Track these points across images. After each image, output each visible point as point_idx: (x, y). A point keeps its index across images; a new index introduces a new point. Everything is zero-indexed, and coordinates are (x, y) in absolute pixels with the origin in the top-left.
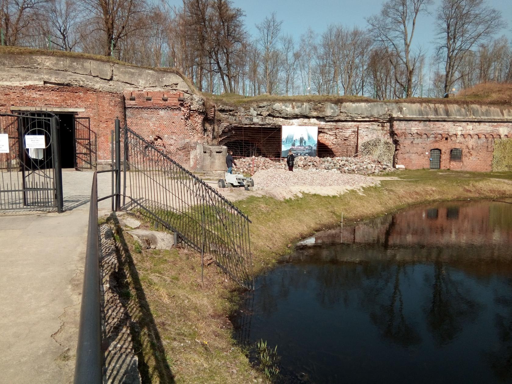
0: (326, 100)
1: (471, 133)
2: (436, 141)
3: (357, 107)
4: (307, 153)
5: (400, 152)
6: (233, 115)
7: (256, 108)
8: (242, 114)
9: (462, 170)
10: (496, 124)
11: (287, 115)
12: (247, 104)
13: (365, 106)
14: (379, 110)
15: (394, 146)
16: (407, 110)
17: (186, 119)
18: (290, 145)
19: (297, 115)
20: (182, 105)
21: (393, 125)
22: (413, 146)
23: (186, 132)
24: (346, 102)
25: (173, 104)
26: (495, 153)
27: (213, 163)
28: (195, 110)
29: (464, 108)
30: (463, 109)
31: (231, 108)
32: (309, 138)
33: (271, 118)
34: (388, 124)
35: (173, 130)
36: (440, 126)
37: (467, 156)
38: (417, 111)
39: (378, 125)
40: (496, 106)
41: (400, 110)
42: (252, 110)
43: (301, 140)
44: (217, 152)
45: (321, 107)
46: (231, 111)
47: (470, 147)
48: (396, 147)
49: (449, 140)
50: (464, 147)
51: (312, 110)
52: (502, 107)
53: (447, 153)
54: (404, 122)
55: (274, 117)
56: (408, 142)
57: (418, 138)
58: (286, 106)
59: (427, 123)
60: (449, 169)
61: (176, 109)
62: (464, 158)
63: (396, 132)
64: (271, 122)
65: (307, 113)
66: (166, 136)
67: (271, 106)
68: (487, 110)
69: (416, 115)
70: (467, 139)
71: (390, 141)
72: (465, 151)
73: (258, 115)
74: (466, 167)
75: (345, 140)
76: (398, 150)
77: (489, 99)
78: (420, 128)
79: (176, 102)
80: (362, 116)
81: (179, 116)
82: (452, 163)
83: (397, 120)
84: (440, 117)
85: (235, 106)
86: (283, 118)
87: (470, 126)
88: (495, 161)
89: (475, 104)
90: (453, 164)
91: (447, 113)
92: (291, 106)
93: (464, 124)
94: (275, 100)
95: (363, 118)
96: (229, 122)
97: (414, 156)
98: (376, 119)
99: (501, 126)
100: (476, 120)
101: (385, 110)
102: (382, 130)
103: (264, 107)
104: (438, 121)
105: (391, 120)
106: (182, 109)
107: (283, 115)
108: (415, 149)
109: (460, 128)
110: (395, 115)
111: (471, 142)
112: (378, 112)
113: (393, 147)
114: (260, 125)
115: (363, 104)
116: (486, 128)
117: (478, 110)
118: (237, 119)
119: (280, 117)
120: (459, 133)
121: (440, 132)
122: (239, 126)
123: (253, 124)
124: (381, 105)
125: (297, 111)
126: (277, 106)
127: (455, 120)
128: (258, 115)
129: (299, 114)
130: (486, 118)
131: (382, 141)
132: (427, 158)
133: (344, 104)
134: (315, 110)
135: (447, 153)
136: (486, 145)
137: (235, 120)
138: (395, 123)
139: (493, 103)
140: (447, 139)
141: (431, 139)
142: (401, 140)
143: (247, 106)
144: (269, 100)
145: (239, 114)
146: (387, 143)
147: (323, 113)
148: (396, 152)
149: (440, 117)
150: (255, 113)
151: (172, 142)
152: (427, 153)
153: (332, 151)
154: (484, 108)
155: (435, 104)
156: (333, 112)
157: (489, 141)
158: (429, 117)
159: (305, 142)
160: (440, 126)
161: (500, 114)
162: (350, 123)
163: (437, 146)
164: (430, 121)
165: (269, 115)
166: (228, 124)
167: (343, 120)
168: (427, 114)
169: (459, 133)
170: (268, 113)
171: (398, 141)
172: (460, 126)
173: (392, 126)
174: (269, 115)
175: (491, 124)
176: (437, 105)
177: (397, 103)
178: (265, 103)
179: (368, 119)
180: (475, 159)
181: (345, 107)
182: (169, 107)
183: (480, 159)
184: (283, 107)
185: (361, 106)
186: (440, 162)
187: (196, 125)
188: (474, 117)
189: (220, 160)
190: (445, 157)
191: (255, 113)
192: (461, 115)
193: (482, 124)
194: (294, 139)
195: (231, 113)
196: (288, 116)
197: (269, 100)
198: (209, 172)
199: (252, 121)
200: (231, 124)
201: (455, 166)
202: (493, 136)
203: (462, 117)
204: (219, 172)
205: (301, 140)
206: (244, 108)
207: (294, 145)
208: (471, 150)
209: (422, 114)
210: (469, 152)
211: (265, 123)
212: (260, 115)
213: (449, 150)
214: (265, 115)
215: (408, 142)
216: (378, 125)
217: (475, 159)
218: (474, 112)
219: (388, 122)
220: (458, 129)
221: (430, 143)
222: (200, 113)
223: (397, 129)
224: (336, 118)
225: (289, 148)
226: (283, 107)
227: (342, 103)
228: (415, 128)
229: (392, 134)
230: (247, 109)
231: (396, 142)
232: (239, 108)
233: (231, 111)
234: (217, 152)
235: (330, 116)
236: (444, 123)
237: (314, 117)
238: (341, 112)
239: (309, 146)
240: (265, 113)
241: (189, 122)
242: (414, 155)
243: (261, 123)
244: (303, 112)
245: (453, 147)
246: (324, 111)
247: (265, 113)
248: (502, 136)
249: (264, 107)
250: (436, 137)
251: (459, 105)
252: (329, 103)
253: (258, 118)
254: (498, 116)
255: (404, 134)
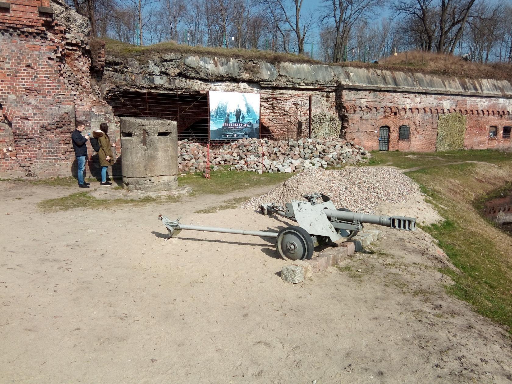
0: (259, 57)
1: (419, 106)
2: (386, 117)
3: (298, 69)
4: (246, 134)
5: (349, 131)
6: (122, 72)
7: (158, 62)
8: (136, 71)
9: (410, 150)
10: (440, 96)
11: (208, 75)
12: (144, 55)
13: (308, 69)
14: (327, 75)
15: (341, 123)
16: (355, 77)
17: (61, 60)
18: (222, 121)
19: (222, 76)
20: (49, 26)
21: (341, 95)
22: (363, 123)
23: (62, 89)
24: (285, 62)
25: (26, 22)
26: (440, 131)
27: (151, 158)
28: (76, 45)
29: (410, 77)
30: (409, 78)
31: (117, 60)
32: (249, 110)
33: (184, 80)
34: (334, 94)
35: (29, 85)
36: (390, 97)
37: (414, 134)
38: (365, 77)
39: (323, 96)
40: (437, 76)
41: (348, 76)
42: (151, 64)
43: (238, 114)
44: (160, 134)
45: (254, 67)
46: (117, 64)
47: (417, 123)
48: (342, 125)
49: (398, 115)
50: (412, 124)
51: (242, 70)
52: (443, 77)
53: (396, 131)
54: (353, 92)
55: (187, 77)
56: (357, 117)
57: (367, 113)
58: (205, 62)
59: (377, 93)
60: (397, 151)
61: (34, 35)
62: (412, 138)
63: (345, 105)
64: (183, 85)
65: (235, 73)
66: (12, 97)
67: (183, 60)
68: (431, 81)
69: (365, 83)
70: (414, 114)
71: (336, 116)
72: (413, 127)
73: (162, 73)
74: (413, 147)
75: (285, 115)
76: (346, 128)
77: (429, 69)
78: (370, 100)
79: (32, 16)
80: (307, 82)
81: (41, 51)
82: (401, 143)
83: (346, 89)
84: (389, 86)
85: (123, 56)
86: (200, 79)
87: (418, 98)
88: (439, 138)
89: (419, 72)
90: (401, 145)
91: (395, 80)
92: (212, 62)
93: (412, 95)
94: (188, 52)
95: (307, 84)
96: (114, 83)
97: (363, 136)
98: (321, 87)
99: (444, 99)
100: (424, 91)
101: (331, 76)
102: (327, 101)
103: (171, 61)
104: (388, 91)
105: (339, 89)
106: (50, 35)
107: (202, 75)
108: (364, 126)
109: (409, 101)
110: (343, 83)
111: (418, 118)
112: (324, 77)
113: (339, 124)
114: (167, 89)
115: (305, 66)
116: (431, 101)
117: (423, 80)
118: (128, 79)
119: (197, 79)
120: (408, 107)
121: (390, 105)
122: (132, 90)
123: (155, 88)
124: (326, 68)
125: (222, 70)
126: (192, 60)
127: (405, 90)
128: (162, 73)
129: (224, 74)
130: (432, 89)
131: (327, 117)
132: (376, 137)
133: (283, 64)
134: (247, 70)
135: (396, 131)
136: (431, 120)
137: (125, 80)
138: (345, 93)
139: (434, 72)
140: (396, 114)
141: (381, 114)
142: (349, 114)
143: (143, 58)
144: (179, 51)
145: (130, 69)
146: (332, 119)
147: (258, 75)
148: (344, 131)
149: (389, 86)
150: (157, 70)
151: (30, 111)
152: (376, 132)
153: (269, 131)
154: (428, 78)
155: (381, 70)
156: (270, 75)
157: (434, 117)
158: (379, 86)
159: (243, 117)
160: (390, 97)
161: (443, 85)
162: (290, 92)
163: (386, 122)
164: (380, 91)
165: (180, 75)
166: (113, 86)
167: (283, 86)
168: (376, 83)
169: (408, 107)
170: (178, 71)
171: (346, 116)
172: (409, 98)
173: (339, 97)
174: (180, 75)
175: (436, 96)
176: (384, 71)
177: (343, 67)
178: (172, 56)
179: (312, 87)
180: (421, 138)
181: (284, 69)
182: (15, 29)
183: (426, 137)
184: (202, 63)
185: (303, 68)
186: (389, 141)
187: (79, 76)
188: (421, 88)
189: (166, 151)
190: (394, 135)
191: (157, 70)
192: (408, 85)
193: (429, 96)
194: (228, 111)
195: (117, 67)
196: (210, 77)
197: (179, 51)
198: (141, 181)
199: (153, 81)
200: (118, 87)
201: (403, 146)
202: (438, 111)
203: (410, 88)
204: (165, 178)
205: (238, 114)
206: (137, 60)
207: (227, 121)
208: (418, 127)
209: (371, 83)
210: (416, 130)
211: (173, 86)
212: (167, 74)
213: (398, 127)
214: (173, 75)
215: (357, 117)
216: (323, 96)
217: (421, 138)
218: (420, 83)
219: (334, 91)
220: (405, 102)
221: (378, 120)
222: (87, 53)
223: (346, 101)
224: (274, 84)
225: (220, 126)
226: (202, 63)
227: (279, 62)
228: (366, 99)
229: (340, 107)
230: (143, 63)
231: (343, 118)
232: (129, 60)
233: (117, 64)
234: (160, 134)
235: (267, 81)
236: (394, 94)
237: (244, 81)
238: (280, 75)
239: (249, 123)
240: (172, 70)
241: (65, 68)
242: (363, 134)
243: (167, 86)
244: (230, 72)
245: (402, 124)
246: (259, 72)
247: (174, 71)
248: (445, 111)
249: (171, 61)
250: (385, 112)
251: (405, 73)
252: (264, 62)
253: (162, 79)
254: (442, 87)
255: (354, 107)
